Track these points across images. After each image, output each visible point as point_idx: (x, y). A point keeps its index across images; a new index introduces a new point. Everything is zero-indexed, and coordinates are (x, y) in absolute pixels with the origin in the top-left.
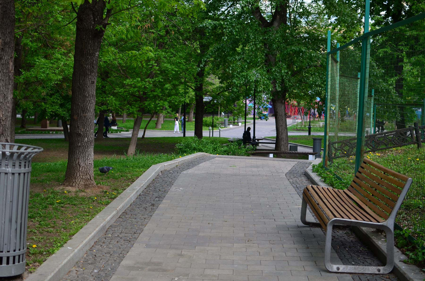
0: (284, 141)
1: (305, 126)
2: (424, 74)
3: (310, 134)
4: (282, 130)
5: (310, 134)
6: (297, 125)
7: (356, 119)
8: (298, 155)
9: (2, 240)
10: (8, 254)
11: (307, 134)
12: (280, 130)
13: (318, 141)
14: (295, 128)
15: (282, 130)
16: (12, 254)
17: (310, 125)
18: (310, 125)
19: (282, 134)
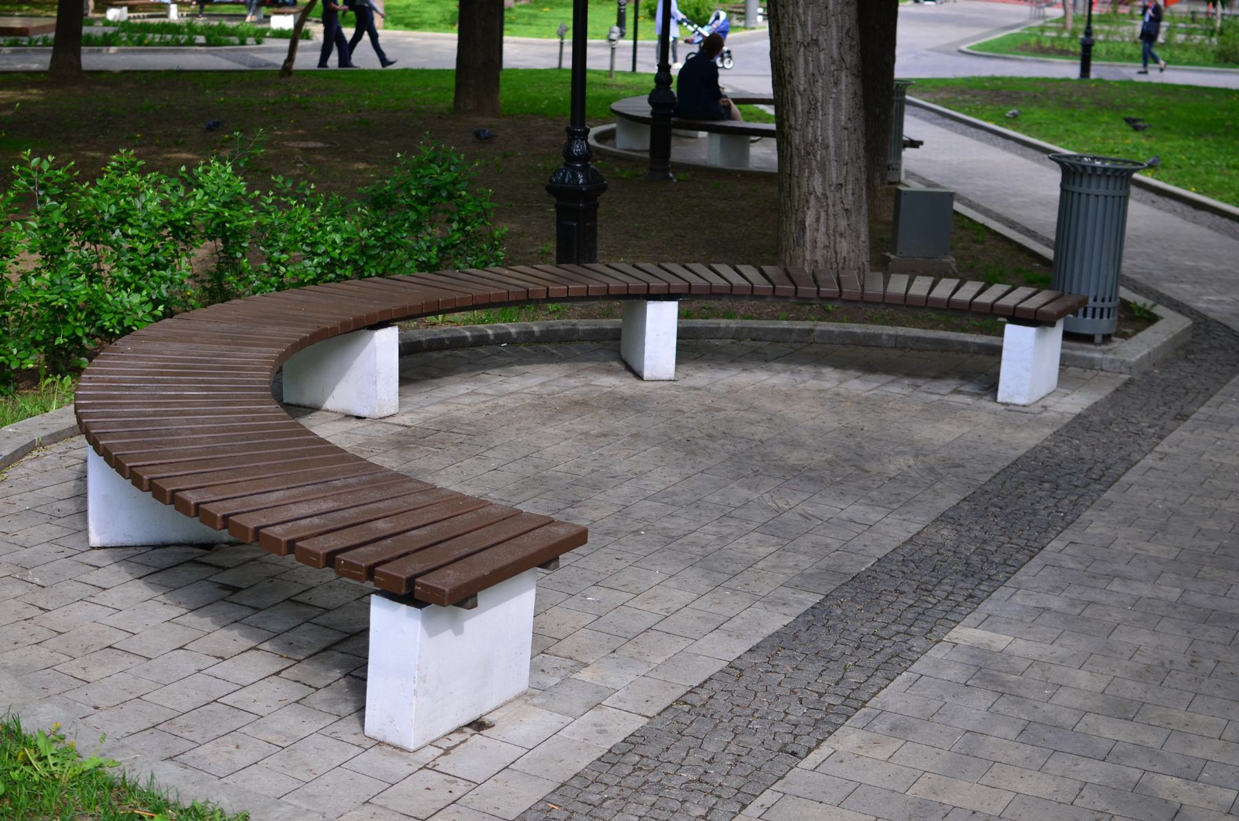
0: (823, 170)
1: (1074, 34)
2: (2, 268)
3: (1085, 70)
4: (812, 81)
5: (1085, 70)
6: (1042, 29)
7: (713, 332)
8: (1209, 97)
9: (754, 72)
10: (1095, 305)
11: (1069, 69)
12: (801, 81)
13: (1098, 188)
14: (1033, 40)
15: (812, 81)
16: (1099, 304)
17: (1088, 32)
18: (1088, 32)
19: (812, 108)
